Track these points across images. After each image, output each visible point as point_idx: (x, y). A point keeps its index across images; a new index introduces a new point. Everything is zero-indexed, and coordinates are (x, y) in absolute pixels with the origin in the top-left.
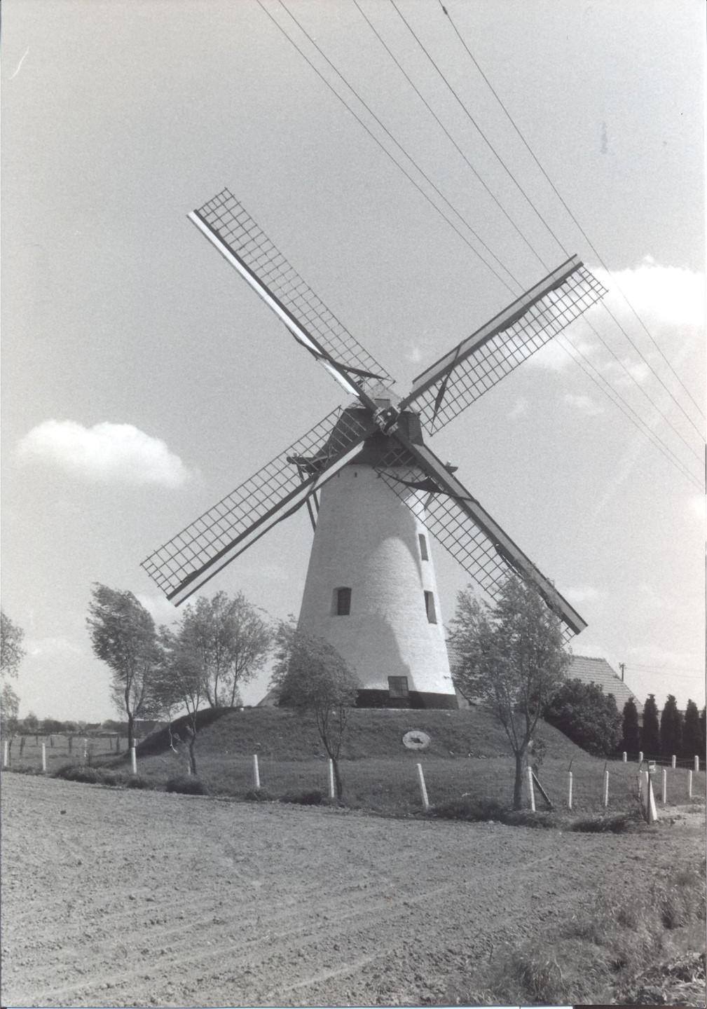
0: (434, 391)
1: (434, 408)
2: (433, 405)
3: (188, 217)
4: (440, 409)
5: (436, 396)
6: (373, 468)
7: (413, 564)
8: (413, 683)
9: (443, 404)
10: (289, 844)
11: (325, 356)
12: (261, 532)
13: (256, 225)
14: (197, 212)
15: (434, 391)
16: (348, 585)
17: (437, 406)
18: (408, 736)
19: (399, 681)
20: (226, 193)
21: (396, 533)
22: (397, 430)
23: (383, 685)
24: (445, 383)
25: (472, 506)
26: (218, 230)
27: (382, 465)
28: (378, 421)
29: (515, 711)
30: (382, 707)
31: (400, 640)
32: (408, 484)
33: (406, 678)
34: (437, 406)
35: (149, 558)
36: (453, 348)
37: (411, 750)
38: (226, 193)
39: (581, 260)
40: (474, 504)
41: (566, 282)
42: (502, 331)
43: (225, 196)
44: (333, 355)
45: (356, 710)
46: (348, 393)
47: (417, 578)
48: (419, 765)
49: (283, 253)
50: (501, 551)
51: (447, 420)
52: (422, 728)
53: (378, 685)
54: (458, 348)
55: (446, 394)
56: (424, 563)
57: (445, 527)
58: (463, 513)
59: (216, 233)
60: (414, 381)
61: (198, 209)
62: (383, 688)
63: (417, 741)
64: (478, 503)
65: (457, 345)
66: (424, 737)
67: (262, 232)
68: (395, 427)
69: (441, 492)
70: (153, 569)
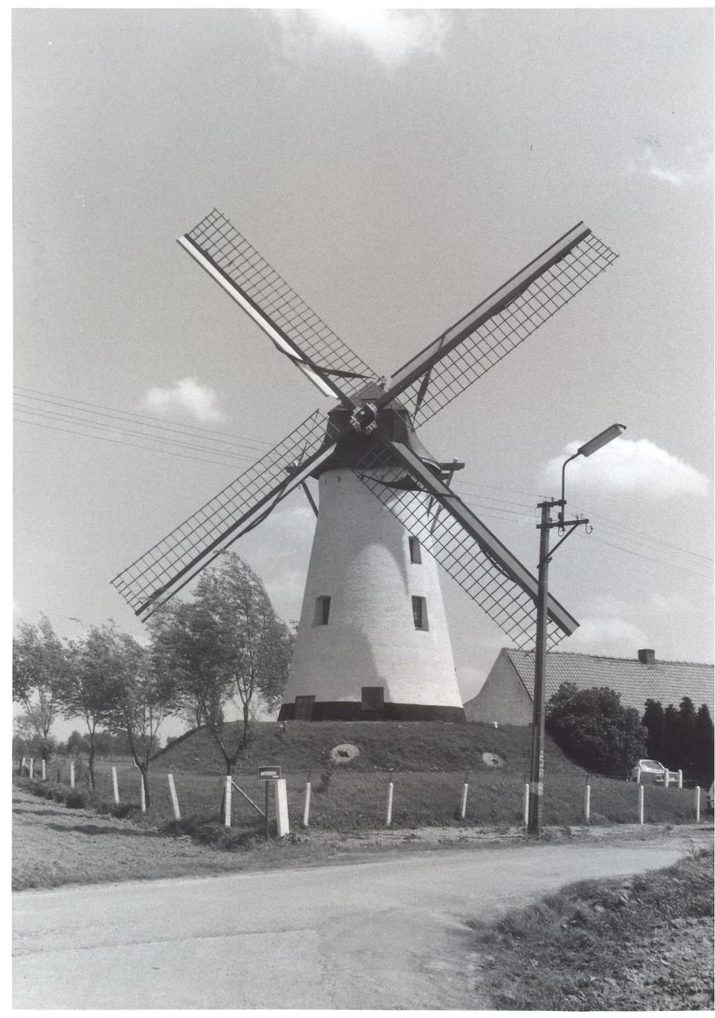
0: (417, 385)
1: (415, 402)
2: (415, 399)
3: (178, 241)
4: (423, 403)
5: (418, 390)
6: (353, 471)
7: (399, 577)
8: (388, 696)
9: (427, 397)
10: (518, 835)
11: (306, 360)
12: (228, 543)
13: (291, 290)
14: (187, 236)
15: (417, 385)
16: (327, 594)
17: (420, 400)
18: (335, 750)
19: (374, 694)
20: (216, 214)
21: (379, 540)
22: (375, 430)
23: (356, 698)
24: (428, 375)
25: (453, 502)
26: (207, 250)
27: (362, 467)
28: (351, 421)
29: (126, 647)
30: (352, 721)
31: (376, 649)
32: (388, 485)
33: (382, 688)
34: (420, 400)
35: (119, 576)
36: (438, 336)
37: (341, 765)
38: (216, 214)
39: (589, 227)
40: (454, 500)
41: (570, 253)
42: (496, 314)
43: (215, 216)
44: (314, 360)
45: (309, 724)
46: (327, 396)
47: (401, 583)
48: (170, 776)
49: (277, 270)
50: (485, 548)
51: (251, 250)
52: (356, 742)
53: (347, 698)
54: (443, 337)
55: (431, 387)
56: (412, 568)
57: (481, 565)
58: (457, 524)
59: (205, 254)
60: (392, 377)
61: (188, 233)
62: (355, 700)
63: (344, 754)
64: (458, 499)
65: (441, 333)
66: (352, 750)
67: (268, 265)
68: (373, 426)
69: (421, 490)
70: (123, 586)
